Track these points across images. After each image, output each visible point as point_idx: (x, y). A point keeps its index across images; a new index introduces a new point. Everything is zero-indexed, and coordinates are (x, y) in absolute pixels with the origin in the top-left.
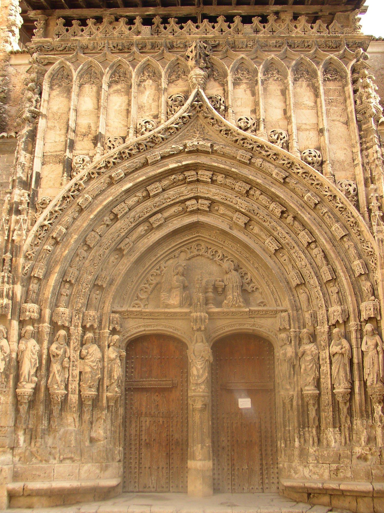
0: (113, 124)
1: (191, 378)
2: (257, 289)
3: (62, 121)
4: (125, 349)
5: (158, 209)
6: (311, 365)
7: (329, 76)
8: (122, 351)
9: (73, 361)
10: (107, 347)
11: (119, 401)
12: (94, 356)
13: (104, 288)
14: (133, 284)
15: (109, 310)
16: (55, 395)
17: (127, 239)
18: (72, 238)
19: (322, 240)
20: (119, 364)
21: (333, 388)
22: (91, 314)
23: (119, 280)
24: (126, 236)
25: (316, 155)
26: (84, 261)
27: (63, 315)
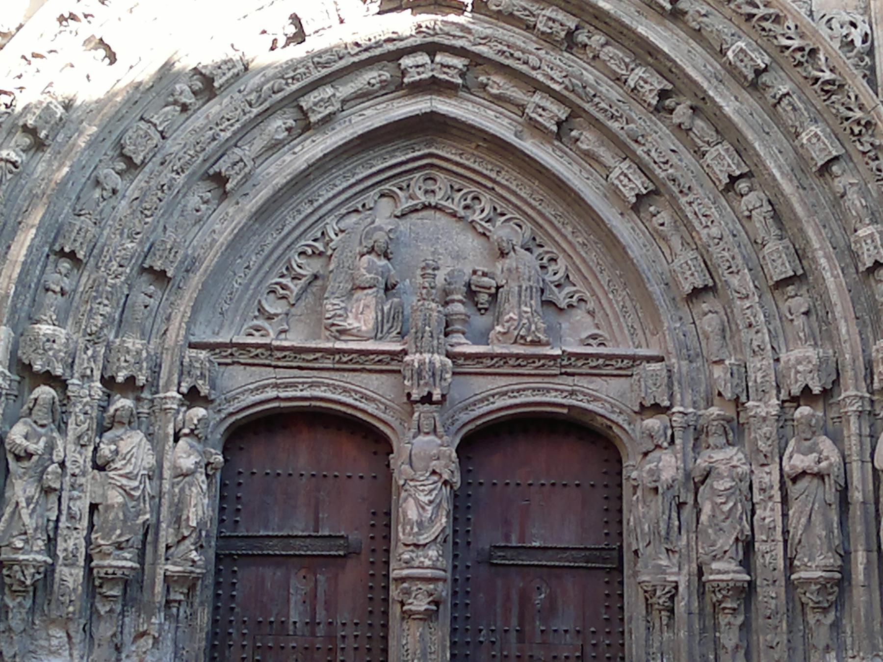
1: (400, 529)
2: (581, 300)
4: (221, 446)
5: (324, 72)
6: (731, 504)
8: (213, 451)
9: (73, 475)
10: (171, 439)
11: (198, 588)
12: (133, 460)
13: (170, 279)
14: (250, 273)
15: (181, 338)
16: (16, 568)
18: (81, 133)
19: (776, 167)
20: (205, 487)
21: (790, 566)
22: (130, 345)
23: (210, 260)
24: (236, 140)
26: (113, 201)
27: (48, 345)
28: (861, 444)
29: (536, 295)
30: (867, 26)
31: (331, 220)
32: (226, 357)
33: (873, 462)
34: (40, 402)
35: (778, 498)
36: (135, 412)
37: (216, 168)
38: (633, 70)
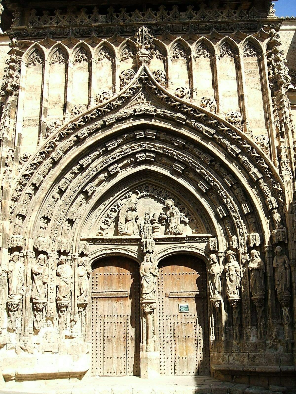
3: (37, 92)
7: (248, 52)
14: (97, 217)
21: (251, 296)
28: (269, 260)
30: (268, 139)
31: (119, 201)
32: (91, 242)
34: (41, 259)
35: (247, 276)
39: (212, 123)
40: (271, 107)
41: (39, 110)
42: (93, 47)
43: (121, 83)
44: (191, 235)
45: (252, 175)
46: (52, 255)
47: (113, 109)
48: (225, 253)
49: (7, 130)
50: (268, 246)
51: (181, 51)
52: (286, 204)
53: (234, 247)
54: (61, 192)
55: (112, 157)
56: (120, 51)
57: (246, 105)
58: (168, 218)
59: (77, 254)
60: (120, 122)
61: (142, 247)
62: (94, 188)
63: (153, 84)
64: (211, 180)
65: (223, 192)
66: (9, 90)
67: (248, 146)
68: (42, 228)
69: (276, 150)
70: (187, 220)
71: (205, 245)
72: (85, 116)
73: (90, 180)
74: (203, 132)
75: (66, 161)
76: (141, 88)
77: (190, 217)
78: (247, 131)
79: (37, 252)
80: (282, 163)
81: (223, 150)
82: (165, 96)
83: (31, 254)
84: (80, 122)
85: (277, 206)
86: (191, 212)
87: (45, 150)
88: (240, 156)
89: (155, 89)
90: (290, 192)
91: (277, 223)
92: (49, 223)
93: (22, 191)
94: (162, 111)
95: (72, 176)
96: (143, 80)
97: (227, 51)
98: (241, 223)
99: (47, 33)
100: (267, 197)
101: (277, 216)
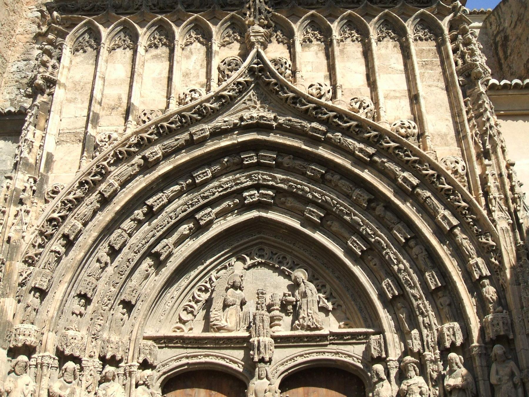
0: (152, 99)
3: (85, 92)
7: (420, 34)
14: (174, 300)
17: (165, 240)
25: (410, 125)
27: (72, 341)
28: (483, 371)
29: (316, 304)
31: (213, 274)
32: (162, 344)
33: (489, 380)
34: (68, 370)
36: (116, 373)
37: (155, 250)
38: (354, 190)
39: (369, 137)
40: (464, 113)
41: (85, 118)
42: (178, 26)
43: (221, 76)
44: (336, 330)
45: (441, 220)
46: (90, 364)
47: (204, 114)
48: (400, 360)
49: (29, 147)
50: (477, 344)
51: (316, 32)
52: (506, 269)
53: (416, 350)
54: (113, 253)
55: (202, 195)
56: (219, 30)
57: (423, 109)
58: (297, 301)
59: (135, 363)
60: (217, 138)
61: (251, 352)
62: (169, 248)
63: (272, 77)
64: (370, 233)
65: (391, 253)
66: (39, 85)
67: (431, 172)
68: (74, 315)
69: (478, 179)
70: (330, 306)
71: (362, 347)
72: (159, 125)
73: (164, 233)
74: (354, 152)
75: (123, 198)
76: (253, 85)
77: (335, 300)
78: (429, 149)
79: (62, 357)
80: (491, 200)
81: (389, 182)
82: (291, 95)
83: (51, 361)
84: (151, 134)
85: (489, 274)
86: (336, 290)
87: (89, 178)
88: (419, 190)
89: (276, 84)
90: (509, 248)
91: (491, 303)
92: (88, 307)
93: (43, 247)
94: (286, 120)
95: (133, 224)
96: (255, 72)
97: (388, 33)
98: (425, 307)
99: (108, 5)
100: (470, 259)
101: (490, 291)
